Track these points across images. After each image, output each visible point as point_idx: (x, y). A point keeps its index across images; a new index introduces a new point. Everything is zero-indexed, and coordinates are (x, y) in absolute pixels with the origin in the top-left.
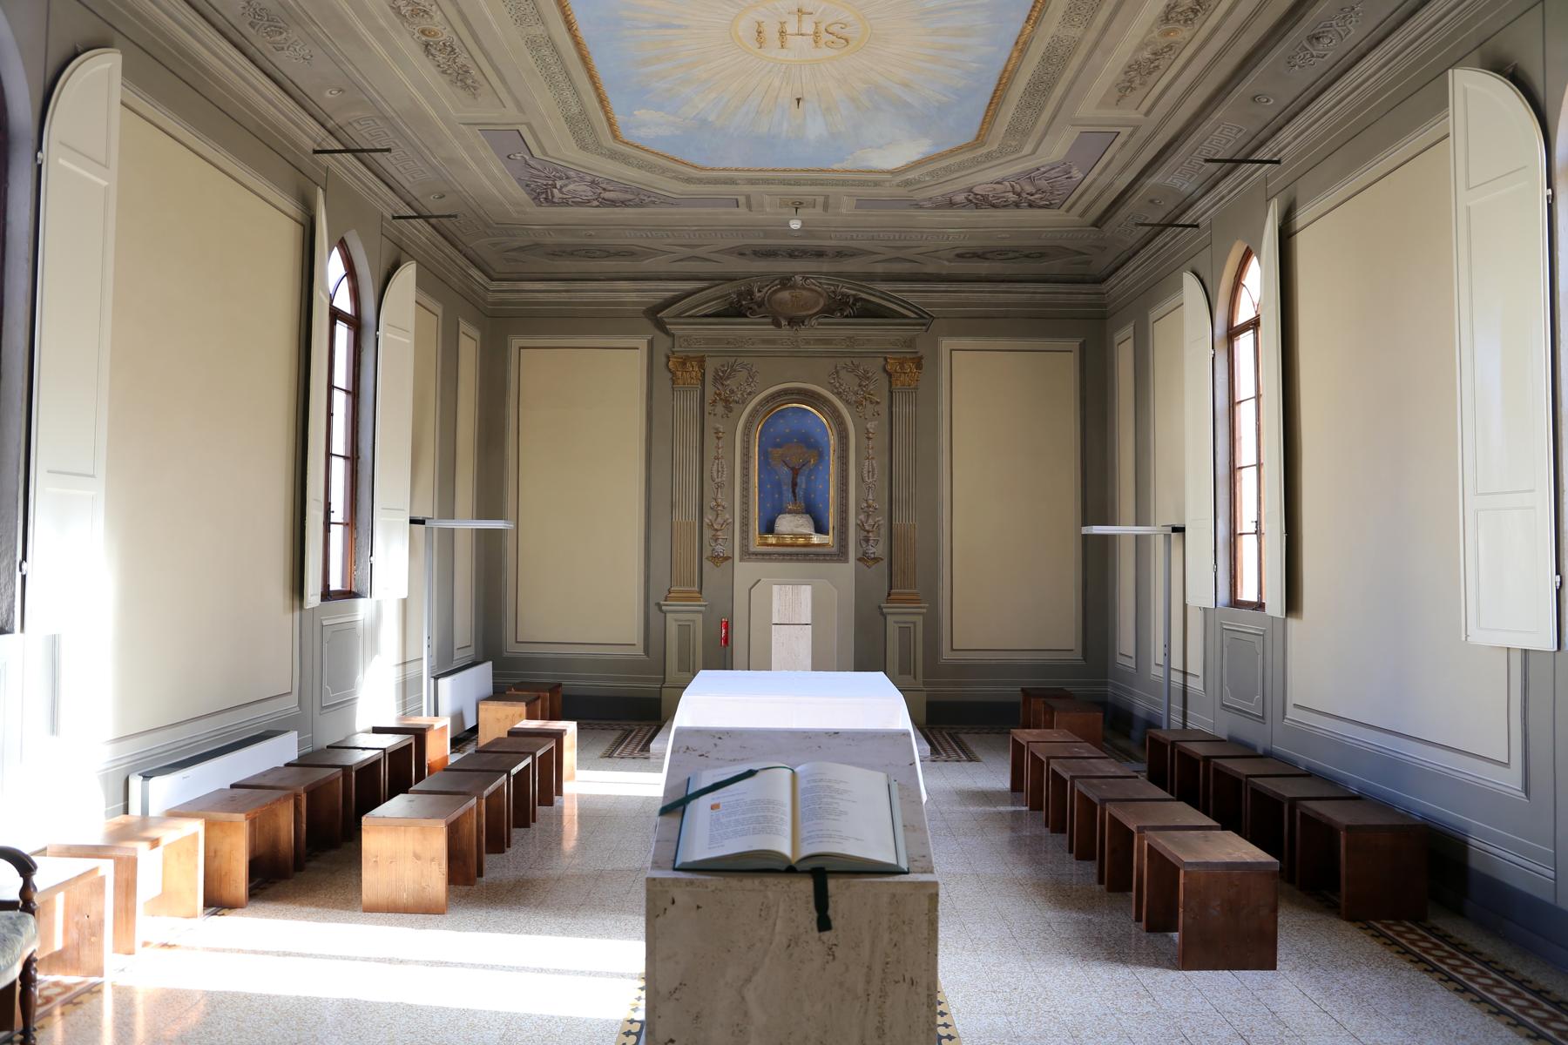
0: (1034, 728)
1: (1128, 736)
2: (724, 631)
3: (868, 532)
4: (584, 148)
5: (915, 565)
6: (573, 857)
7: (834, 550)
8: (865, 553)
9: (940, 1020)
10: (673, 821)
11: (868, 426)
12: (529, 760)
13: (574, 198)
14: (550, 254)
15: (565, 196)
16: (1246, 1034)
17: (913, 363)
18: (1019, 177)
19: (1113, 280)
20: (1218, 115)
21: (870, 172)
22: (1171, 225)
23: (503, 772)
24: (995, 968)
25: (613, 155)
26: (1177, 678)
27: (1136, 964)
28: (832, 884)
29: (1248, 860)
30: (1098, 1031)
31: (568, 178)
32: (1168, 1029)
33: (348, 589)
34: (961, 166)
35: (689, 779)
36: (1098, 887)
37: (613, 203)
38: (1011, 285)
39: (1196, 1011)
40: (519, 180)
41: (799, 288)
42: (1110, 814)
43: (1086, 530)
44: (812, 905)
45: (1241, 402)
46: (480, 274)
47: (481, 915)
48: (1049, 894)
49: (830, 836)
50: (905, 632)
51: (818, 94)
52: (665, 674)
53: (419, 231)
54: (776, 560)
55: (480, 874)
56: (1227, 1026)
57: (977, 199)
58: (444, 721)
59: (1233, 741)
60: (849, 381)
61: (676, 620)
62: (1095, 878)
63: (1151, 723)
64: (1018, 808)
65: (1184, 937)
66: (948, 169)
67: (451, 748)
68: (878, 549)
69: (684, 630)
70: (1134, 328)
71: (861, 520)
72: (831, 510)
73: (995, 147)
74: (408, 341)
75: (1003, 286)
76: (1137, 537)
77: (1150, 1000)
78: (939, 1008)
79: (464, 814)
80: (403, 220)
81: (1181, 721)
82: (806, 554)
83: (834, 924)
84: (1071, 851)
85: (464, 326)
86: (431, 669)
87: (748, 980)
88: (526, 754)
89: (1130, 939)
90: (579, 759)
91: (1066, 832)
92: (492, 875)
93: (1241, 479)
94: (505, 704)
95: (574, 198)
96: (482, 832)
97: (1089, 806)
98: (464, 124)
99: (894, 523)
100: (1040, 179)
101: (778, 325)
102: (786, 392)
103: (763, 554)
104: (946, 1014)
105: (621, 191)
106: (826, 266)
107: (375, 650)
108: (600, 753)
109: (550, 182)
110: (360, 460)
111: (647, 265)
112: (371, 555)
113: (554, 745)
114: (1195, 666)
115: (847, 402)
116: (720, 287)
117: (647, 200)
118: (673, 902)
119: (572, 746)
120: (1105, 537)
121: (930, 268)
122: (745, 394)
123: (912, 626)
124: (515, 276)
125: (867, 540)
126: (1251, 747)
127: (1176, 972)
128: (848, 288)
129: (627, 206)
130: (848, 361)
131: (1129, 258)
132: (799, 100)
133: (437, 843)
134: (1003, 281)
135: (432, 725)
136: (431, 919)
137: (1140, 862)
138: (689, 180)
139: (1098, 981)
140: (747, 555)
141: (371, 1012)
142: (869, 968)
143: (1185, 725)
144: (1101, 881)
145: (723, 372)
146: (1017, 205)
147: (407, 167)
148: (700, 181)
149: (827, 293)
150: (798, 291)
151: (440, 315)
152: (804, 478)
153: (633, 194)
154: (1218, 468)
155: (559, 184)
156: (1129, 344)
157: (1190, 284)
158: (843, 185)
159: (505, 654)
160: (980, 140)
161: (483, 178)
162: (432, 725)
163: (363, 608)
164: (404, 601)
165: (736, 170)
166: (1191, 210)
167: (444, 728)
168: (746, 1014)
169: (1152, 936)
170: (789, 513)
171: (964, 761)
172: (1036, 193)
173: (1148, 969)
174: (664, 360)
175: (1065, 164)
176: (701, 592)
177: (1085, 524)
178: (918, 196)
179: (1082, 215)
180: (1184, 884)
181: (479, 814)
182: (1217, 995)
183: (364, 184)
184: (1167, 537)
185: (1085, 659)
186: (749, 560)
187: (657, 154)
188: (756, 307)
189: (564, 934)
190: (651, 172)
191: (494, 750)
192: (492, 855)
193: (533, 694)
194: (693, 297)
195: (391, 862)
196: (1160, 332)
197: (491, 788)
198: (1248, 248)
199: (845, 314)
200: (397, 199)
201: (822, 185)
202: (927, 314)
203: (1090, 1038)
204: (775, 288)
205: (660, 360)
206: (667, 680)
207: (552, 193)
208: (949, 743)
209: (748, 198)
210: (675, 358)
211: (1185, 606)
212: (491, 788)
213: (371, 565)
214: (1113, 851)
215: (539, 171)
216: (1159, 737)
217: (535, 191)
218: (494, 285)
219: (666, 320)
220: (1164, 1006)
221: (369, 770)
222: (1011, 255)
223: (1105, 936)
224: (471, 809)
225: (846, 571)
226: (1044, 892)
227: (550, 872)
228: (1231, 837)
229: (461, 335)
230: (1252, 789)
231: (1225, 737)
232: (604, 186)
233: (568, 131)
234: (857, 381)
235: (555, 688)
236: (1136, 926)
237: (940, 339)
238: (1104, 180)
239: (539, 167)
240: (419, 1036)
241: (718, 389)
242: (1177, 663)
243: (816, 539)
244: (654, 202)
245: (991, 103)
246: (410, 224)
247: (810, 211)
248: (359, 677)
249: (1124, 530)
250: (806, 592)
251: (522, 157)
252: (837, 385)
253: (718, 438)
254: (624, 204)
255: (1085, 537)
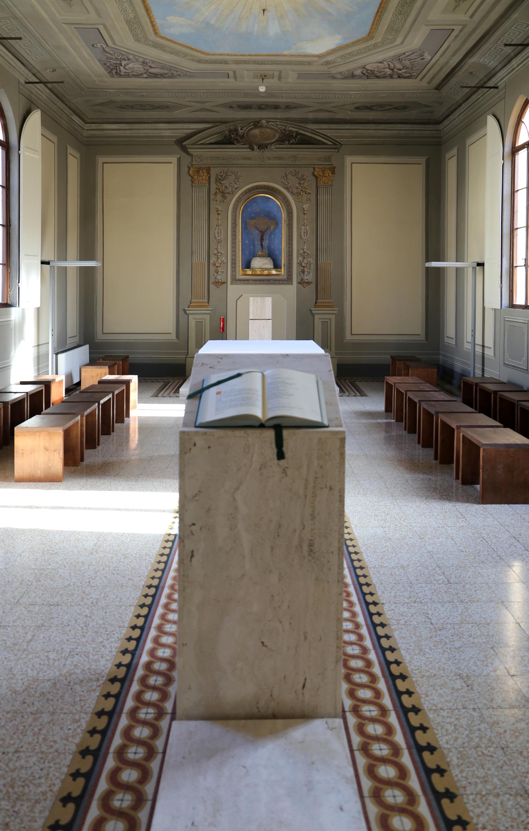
0: (398, 376)
1: (451, 383)
2: (222, 324)
3: (304, 267)
4: (138, 40)
5: (331, 286)
6: (135, 450)
7: (285, 277)
8: (302, 279)
9: (346, 531)
10: (195, 402)
11: (304, 207)
12: (110, 396)
13: (133, 72)
14: (119, 107)
15: (127, 71)
16: (517, 536)
17: (330, 171)
18: (393, 59)
19: (446, 122)
20: (515, 16)
21: (306, 56)
22: (482, 87)
23: (95, 402)
24: (377, 504)
25: (156, 45)
26: (479, 349)
27: (456, 501)
28: (286, 433)
29: (519, 443)
30: (435, 535)
31: (129, 60)
32: (474, 534)
33: (6, 302)
34: (359, 52)
35: (203, 380)
36: (434, 462)
37: (156, 76)
38: (387, 125)
39: (489, 525)
40: (100, 60)
41: (264, 128)
42: (441, 420)
43: (428, 265)
44: (274, 445)
45: (518, 190)
46: (79, 119)
47: (83, 481)
48: (407, 465)
49: (284, 407)
50: (325, 324)
51: (276, 7)
52: (188, 350)
53: (41, 91)
54: (251, 284)
55: (82, 460)
56: (507, 532)
57: (368, 73)
58: (61, 377)
59: (510, 383)
60: (293, 181)
61: (194, 319)
62: (433, 457)
63: (464, 374)
64: (389, 421)
65: (484, 489)
66: (351, 54)
67: (66, 394)
68: (310, 277)
69: (199, 324)
70: (458, 150)
71: (300, 260)
72: (283, 255)
73: (379, 40)
74: (38, 157)
75: (382, 126)
76: (457, 269)
77: (464, 519)
78: (346, 524)
79: (73, 425)
80: (31, 84)
81: (481, 374)
82: (269, 280)
83: (286, 455)
84: (419, 443)
85: (70, 150)
86: (53, 348)
87: (238, 489)
88: (108, 393)
89: (453, 488)
90: (139, 398)
91: (416, 433)
92: (89, 461)
93: (517, 235)
94: (97, 368)
95: (133, 72)
96: (83, 436)
97: (429, 416)
98: (65, 24)
99: (319, 262)
100: (405, 60)
101: (252, 149)
102: (257, 187)
103: (244, 280)
104: (349, 527)
105: (160, 68)
106: (280, 114)
107: (21, 337)
108: (151, 395)
109: (118, 62)
110: (11, 227)
111: (177, 114)
112: (19, 282)
113: (125, 388)
114: (489, 342)
115: (292, 193)
116: (219, 127)
117: (176, 74)
118: (195, 445)
119: (135, 389)
120: (438, 269)
121: (340, 116)
122: (233, 188)
123: (329, 321)
124: (99, 121)
125: (303, 272)
126: (521, 387)
127: (479, 505)
128: (293, 127)
129: (164, 77)
130: (292, 169)
131: (456, 109)
132: (264, 10)
133: (58, 441)
134: (382, 123)
135: (54, 380)
136: (54, 485)
137: (458, 446)
138: (200, 61)
139: (435, 510)
140: (235, 281)
141: (20, 534)
142: (306, 480)
143: (483, 375)
144: (436, 458)
145: (220, 176)
146: (391, 76)
147: (31, 51)
148: (206, 62)
149: (280, 130)
150: (263, 129)
151: (56, 143)
152: (267, 237)
153: (167, 69)
154: (504, 228)
155: (123, 63)
156: (455, 159)
157: (491, 122)
158: (290, 64)
159: (96, 341)
160: (370, 35)
161: (79, 60)
162: (54, 380)
163: (14, 313)
164: (38, 309)
165: (228, 55)
166: (494, 78)
167: (61, 381)
168: (236, 508)
169: (465, 487)
170: (259, 257)
171: (358, 396)
172: (403, 69)
173: (463, 504)
174: (187, 169)
175: (420, 50)
176: (208, 302)
177: (427, 261)
178: (334, 71)
179: (429, 82)
180: (483, 456)
181: (82, 425)
182: (501, 517)
183: (6, 60)
184: (474, 269)
185: (427, 340)
186: (236, 284)
187: (181, 44)
188: (239, 138)
189: (131, 490)
190: (176, 55)
191: (90, 391)
192: (89, 450)
193: (113, 362)
194: (203, 133)
195: (31, 453)
196: (472, 152)
197: (89, 411)
198: (527, 99)
199: (291, 142)
200: (27, 72)
201: (278, 64)
202: (338, 142)
203: (430, 539)
204: (250, 127)
205: (185, 169)
206: (189, 353)
207: (120, 69)
208: (349, 386)
209: (235, 72)
210: (193, 168)
211: (484, 308)
212: (89, 411)
213: (19, 288)
214: (443, 441)
215: (111, 55)
216: (468, 380)
217: (110, 68)
218: (86, 127)
219: (188, 146)
220: (472, 523)
221: (18, 404)
222: (387, 107)
223: (438, 486)
224: (77, 422)
225: (292, 289)
226: (404, 464)
227: (122, 458)
228: (509, 431)
229: (69, 156)
230: (521, 408)
231: (506, 381)
232: (150, 64)
233: (128, 29)
234: (298, 181)
235: (125, 359)
236: (456, 482)
237: (346, 157)
238: (443, 61)
239: (112, 52)
240: (47, 545)
241: (218, 186)
242: (479, 341)
243: (274, 272)
244: (179, 75)
245: (378, 12)
246: (36, 87)
247: (271, 80)
248: (13, 353)
249: (449, 264)
250: (268, 301)
251: (101, 45)
252: (286, 183)
253: (218, 214)
254: (162, 76)
255: (427, 269)
